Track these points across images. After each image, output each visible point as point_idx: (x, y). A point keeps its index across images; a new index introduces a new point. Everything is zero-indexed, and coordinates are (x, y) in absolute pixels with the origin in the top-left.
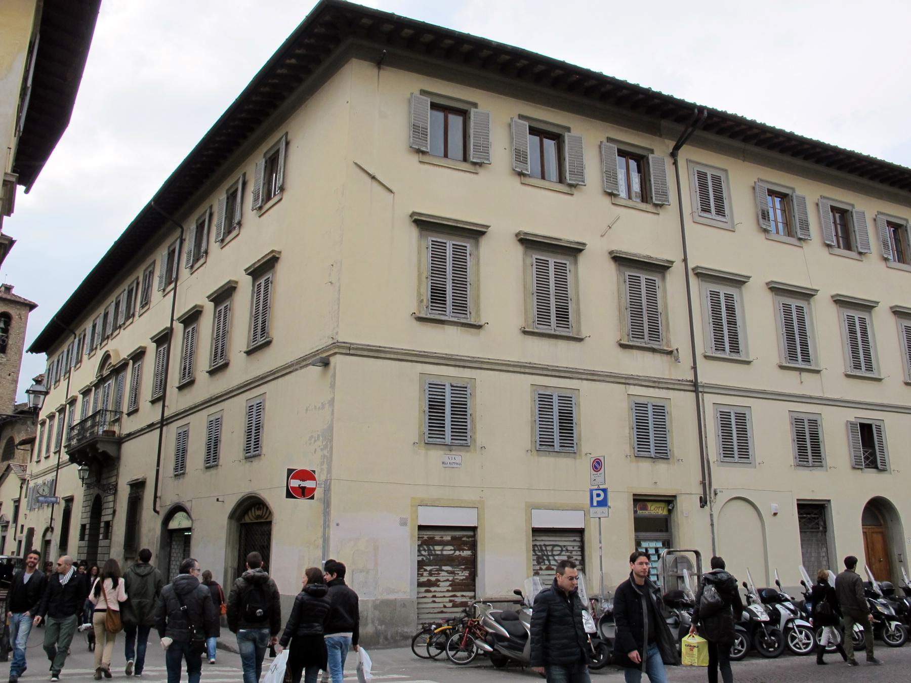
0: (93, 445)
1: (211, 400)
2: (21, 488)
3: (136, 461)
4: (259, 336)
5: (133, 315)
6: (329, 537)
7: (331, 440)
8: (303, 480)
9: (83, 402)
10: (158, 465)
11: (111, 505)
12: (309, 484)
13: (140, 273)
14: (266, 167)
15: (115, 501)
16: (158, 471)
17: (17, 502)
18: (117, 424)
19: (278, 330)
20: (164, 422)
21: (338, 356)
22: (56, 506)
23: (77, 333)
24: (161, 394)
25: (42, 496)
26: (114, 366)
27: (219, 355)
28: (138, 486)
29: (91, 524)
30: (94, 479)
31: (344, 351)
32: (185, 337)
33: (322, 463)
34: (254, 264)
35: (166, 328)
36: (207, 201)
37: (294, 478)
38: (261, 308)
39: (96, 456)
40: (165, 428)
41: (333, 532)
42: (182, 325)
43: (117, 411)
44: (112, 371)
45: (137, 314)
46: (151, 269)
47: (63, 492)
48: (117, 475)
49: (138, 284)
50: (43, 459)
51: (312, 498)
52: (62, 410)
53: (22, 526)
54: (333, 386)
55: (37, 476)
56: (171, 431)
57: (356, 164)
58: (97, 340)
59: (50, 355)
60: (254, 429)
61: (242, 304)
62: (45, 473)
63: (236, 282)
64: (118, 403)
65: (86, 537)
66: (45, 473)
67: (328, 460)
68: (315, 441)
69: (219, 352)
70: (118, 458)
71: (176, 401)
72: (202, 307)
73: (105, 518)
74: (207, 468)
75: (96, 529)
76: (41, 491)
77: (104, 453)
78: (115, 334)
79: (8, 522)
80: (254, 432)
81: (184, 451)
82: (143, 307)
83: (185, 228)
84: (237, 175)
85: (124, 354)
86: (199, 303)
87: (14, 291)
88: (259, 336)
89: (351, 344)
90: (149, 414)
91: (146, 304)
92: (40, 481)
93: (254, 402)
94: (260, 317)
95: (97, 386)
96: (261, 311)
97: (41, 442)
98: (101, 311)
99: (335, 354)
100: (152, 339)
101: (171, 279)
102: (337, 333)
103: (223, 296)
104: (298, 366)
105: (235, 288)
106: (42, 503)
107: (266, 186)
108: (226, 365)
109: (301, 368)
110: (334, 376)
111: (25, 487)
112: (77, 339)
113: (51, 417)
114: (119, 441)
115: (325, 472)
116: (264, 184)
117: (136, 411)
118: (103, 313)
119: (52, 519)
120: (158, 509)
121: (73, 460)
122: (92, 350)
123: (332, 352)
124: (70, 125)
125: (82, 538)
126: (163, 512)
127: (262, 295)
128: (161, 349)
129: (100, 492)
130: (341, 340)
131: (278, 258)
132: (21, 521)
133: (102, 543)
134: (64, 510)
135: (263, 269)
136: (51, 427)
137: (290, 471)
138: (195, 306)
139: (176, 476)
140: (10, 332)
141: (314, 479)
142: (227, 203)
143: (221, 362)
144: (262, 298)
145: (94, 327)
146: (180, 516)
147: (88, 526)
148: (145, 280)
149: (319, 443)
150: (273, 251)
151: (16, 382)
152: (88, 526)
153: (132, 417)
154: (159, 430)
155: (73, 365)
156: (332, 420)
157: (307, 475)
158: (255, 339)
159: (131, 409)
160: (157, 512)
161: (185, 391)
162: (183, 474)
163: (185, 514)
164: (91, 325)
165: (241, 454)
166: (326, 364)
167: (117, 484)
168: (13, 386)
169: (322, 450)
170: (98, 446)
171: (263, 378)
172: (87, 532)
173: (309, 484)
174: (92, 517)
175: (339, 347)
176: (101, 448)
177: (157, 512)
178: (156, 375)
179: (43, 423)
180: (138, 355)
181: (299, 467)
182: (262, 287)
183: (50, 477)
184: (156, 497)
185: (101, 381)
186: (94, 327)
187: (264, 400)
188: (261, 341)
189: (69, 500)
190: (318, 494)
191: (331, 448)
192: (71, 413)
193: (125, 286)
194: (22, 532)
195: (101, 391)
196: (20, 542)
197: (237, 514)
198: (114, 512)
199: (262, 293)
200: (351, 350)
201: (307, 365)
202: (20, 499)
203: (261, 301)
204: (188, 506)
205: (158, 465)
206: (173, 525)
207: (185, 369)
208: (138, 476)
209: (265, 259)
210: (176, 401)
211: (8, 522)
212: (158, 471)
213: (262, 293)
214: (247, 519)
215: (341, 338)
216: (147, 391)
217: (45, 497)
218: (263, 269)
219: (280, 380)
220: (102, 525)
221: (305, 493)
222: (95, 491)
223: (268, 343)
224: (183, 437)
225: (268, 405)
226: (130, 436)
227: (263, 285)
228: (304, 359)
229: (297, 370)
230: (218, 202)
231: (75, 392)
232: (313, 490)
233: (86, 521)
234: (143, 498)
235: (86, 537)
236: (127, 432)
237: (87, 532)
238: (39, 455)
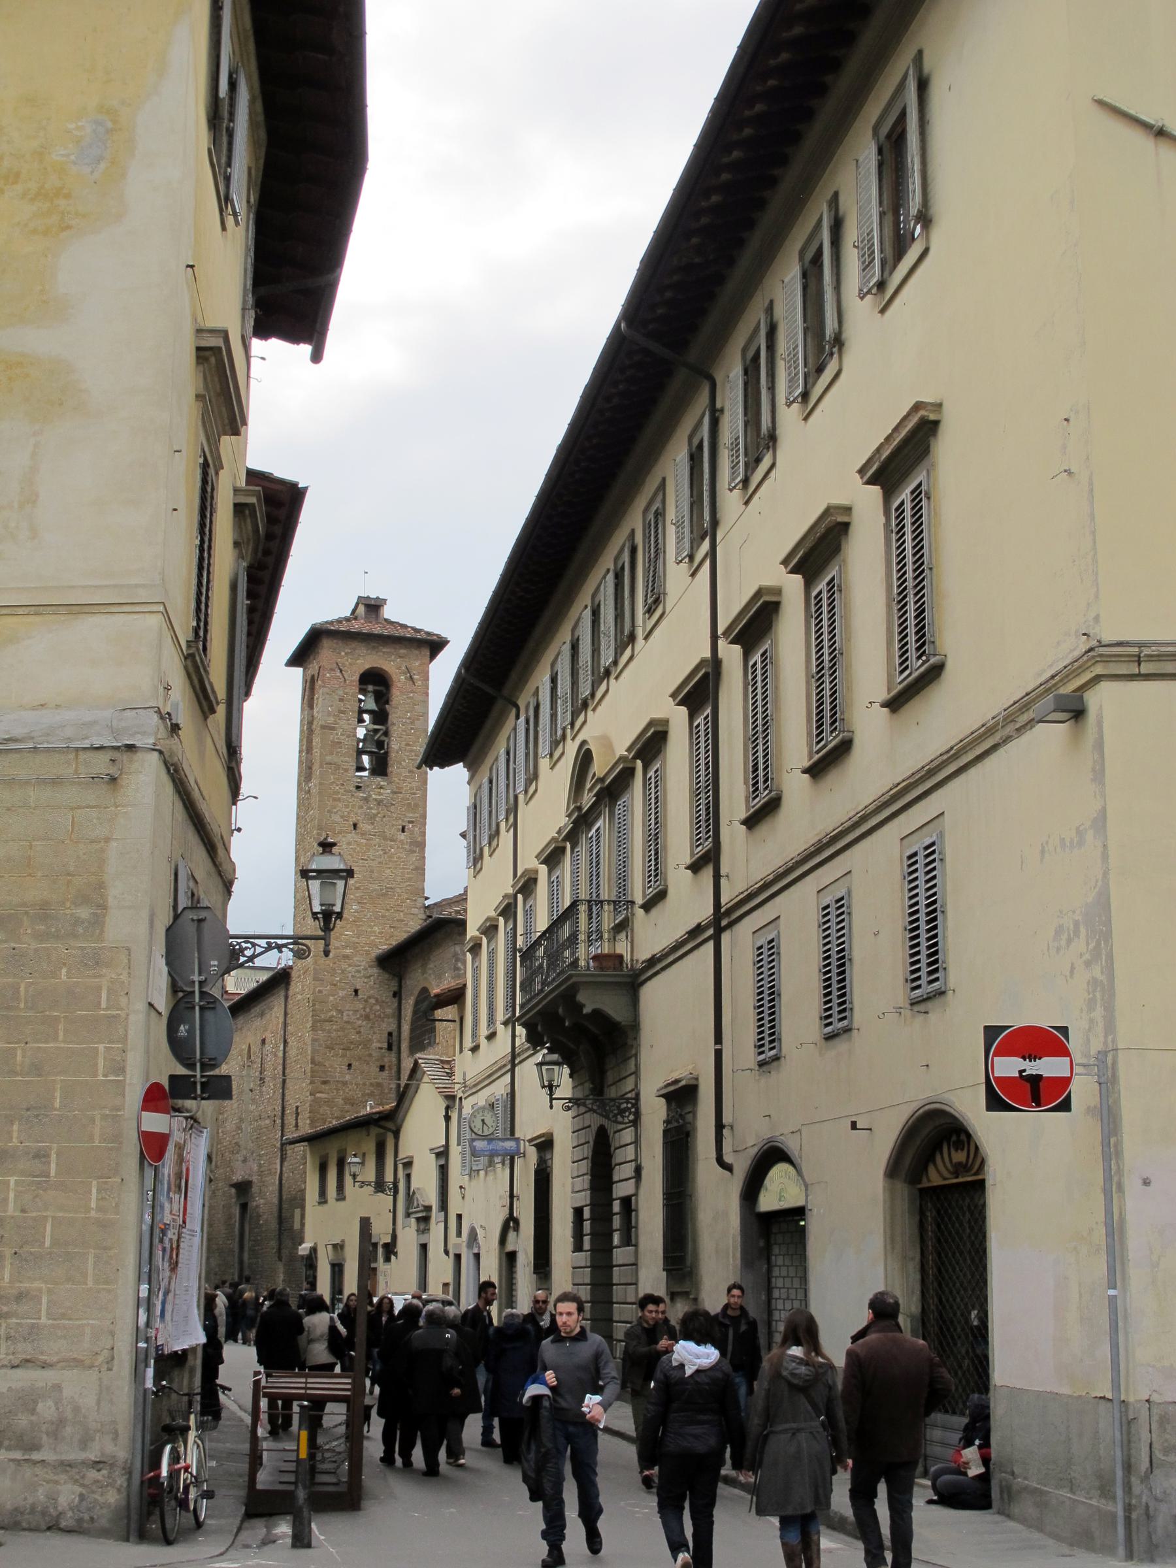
0: (568, 996)
1: (820, 848)
2: (447, 1118)
3: (673, 1033)
4: (912, 654)
5: (632, 638)
6: (1122, 1220)
7: (1107, 936)
8: (1032, 1057)
9: (550, 883)
10: (718, 1039)
11: (630, 1153)
12: (1049, 1067)
13: (635, 521)
14: (881, 165)
15: (636, 1142)
16: (718, 1054)
17: (443, 1154)
18: (623, 935)
19: (956, 634)
20: (722, 920)
21: (1104, 685)
22: (518, 1163)
23: (522, 703)
24: (708, 844)
25: (483, 1137)
26: (602, 780)
27: (827, 720)
28: (681, 1096)
29: (593, 1205)
30: (588, 1085)
31: (1123, 669)
32: (749, 683)
33: (1091, 1004)
34: (878, 450)
35: (703, 662)
36: (759, 293)
37: (1003, 1052)
38: (910, 575)
39: (583, 1028)
40: (726, 937)
41: (1136, 1207)
42: (737, 649)
43: (622, 903)
44: (601, 794)
45: (640, 634)
46: (657, 505)
47: (530, 1124)
48: (636, 1073)
49: (634, 551)
50: (483, 1042)
51: (1065, 1106)
52: (508, 910)
53: (459, 1217)
54: (1099, 775)
55: (476, 1087)
56: (740, 943)
57: (1101, 103)
58: (564, 718)
59: (473, 767)
60: (923, 918)
61: (866, 563)
62: (490, 1078)
63: (848, 510)
64: (622, 879)
65: (587, 1240)
66: (490, 1078)
67: (1104, 993)
68: (1069, 941)
69: (827, 714)
70: (635, 1026)
71: (747, 859)
72: (778, 591)
73: (621, 1190)
74: (829, 1038)
75: (604, 1221)
76: (478, 1125)
77: (597, 1014)
78: (599, 694)
79: (428, 1209)
80: (924, 927)
81: (774, 994)
82: (650, 611)
83: (719, 379)
84: (818, 210)
85: (622, 745)
86: (768, 582)
87: (388, 613)
88: (912, 654)
89: (1141, 645)
90: (689, 902)
91: (657, 601)
92: (481, 1099)
93: (917, 845)
94: (911, 599)
95: (573, 836)
96: (910, 583)
97: (476, 996)
98: (564, 636)
99: (1097, 679)
100: (673, 695)
101: (706, 527)
102: (1097, 619)
103: (819, 552)
104: (1010, 729)
105: (845, 526)
106: (492, 1155)
107: (889, 218)
108: (845, 747)
109: (1020, 731)
110: (1099, 745)
111: (454, 1116)
112: (522, 719)
113: (490, 929)
114: (632, 981)
115: (1100, 1028)
116: (882, 215)
117: (661, 895)
118: (568, 639)
119: (512, 1196)
120: (728, 1158)
121: (535, 1040)
122: (555, 744)
123: (1087, 676)
124: (371, 165)
125: (578, 1247)
126: (742, 1166)
127: (909, 537)
128: (699, 720)
129: (605, 1122)
130: (1108, 638)
131: (936, 424)
132: (454, 1208)
133: (620, 1255)
134: (537, 1172)
135: (904, 459)
136: (492, 954)
137: (991, 1032)
138: (759, 593)
139: (761, 1064)
140: (392, 718)
141: (1064, 1052)
142: (805, 288)
143: (832, 740)
144: (909, 545)
145: (554, 680)
146: (778, 1174)
147: (587, 1213)
148: (647, 537)
149: (1080, 945)
150: (917, 406)
151: (422, 845)
152: (587, 1213)
153: (654, 912)
154: (711, 944)
155: (520, 788)
156: (1106, 874)
157: (1048, 1042)
158: (904, 665)
159: (651, 892)
160: (728, 1168)
161: (763, 829)
162: (777, 1058)
163: (790, 1168)
164: (546, 678)
165: (899, 993)
166: (1077, 713)
167: (637, 1097)
168: (414, 857)
169: (1088, 964)
170: (581, 997)
171: (931, 773)
172: (587, 1225)
173: (1049, 1067)
174: (594, 1188)
175: (1106, 659)
176: (589, 1002)
177: (728, 1168)
178: (696, 793)
179: (476, 948)
180: (652, 743)
181: (1018, 1019)
182: (908, 513)
183: (500, 1088)
184: (720, 1126)
185: (582, 822)
186: (554, 680)
187: (941, 835)
188: (917, 667)
189: (545, 1145)
190: (1082, 1091)
191: (1110, 957)
192: (529, 913)
193: (607, 562)
194: (459, 1234)
195: (583, 848)
196: (458, 1257)
197: (907, 1161)
198: (638, 1170)
199: (908, 529)
200: (1143, 663)
201: (1031, 723)
202: (447, 1146)
203: (909, 552)
204: (791, 1145)
205: (718, 1039)
206: (768, 1202)
207: (755, 769)
208: (680, 1072)
209: (903, 433)
210: (747, 859)
211: (428, 1209)
212: (718, 1054)
213: (908, 529)
214: (935, 1177)
215: (1109, 635)
216: (680, 846)
217: (489, 1139)
218: (904, 459)
219: (973, 771)
220: (616, 1207)
221: (1042, 1094)
222: (595, 1120)
223: (935, 672)
224: (768, 956)
225: (951, 850)
226: (656, 964)
227: (908, 506)
228: (1024, 704)
229: (1007, 740)
230: (784, 288)
231: (529, 861)
232: (1066, 1081)
233: (584, 1199)
234: (695, 1129)
235: (587, 1240)
236: (647, 955)
237: (587, 1225)
238: (475, 1035)
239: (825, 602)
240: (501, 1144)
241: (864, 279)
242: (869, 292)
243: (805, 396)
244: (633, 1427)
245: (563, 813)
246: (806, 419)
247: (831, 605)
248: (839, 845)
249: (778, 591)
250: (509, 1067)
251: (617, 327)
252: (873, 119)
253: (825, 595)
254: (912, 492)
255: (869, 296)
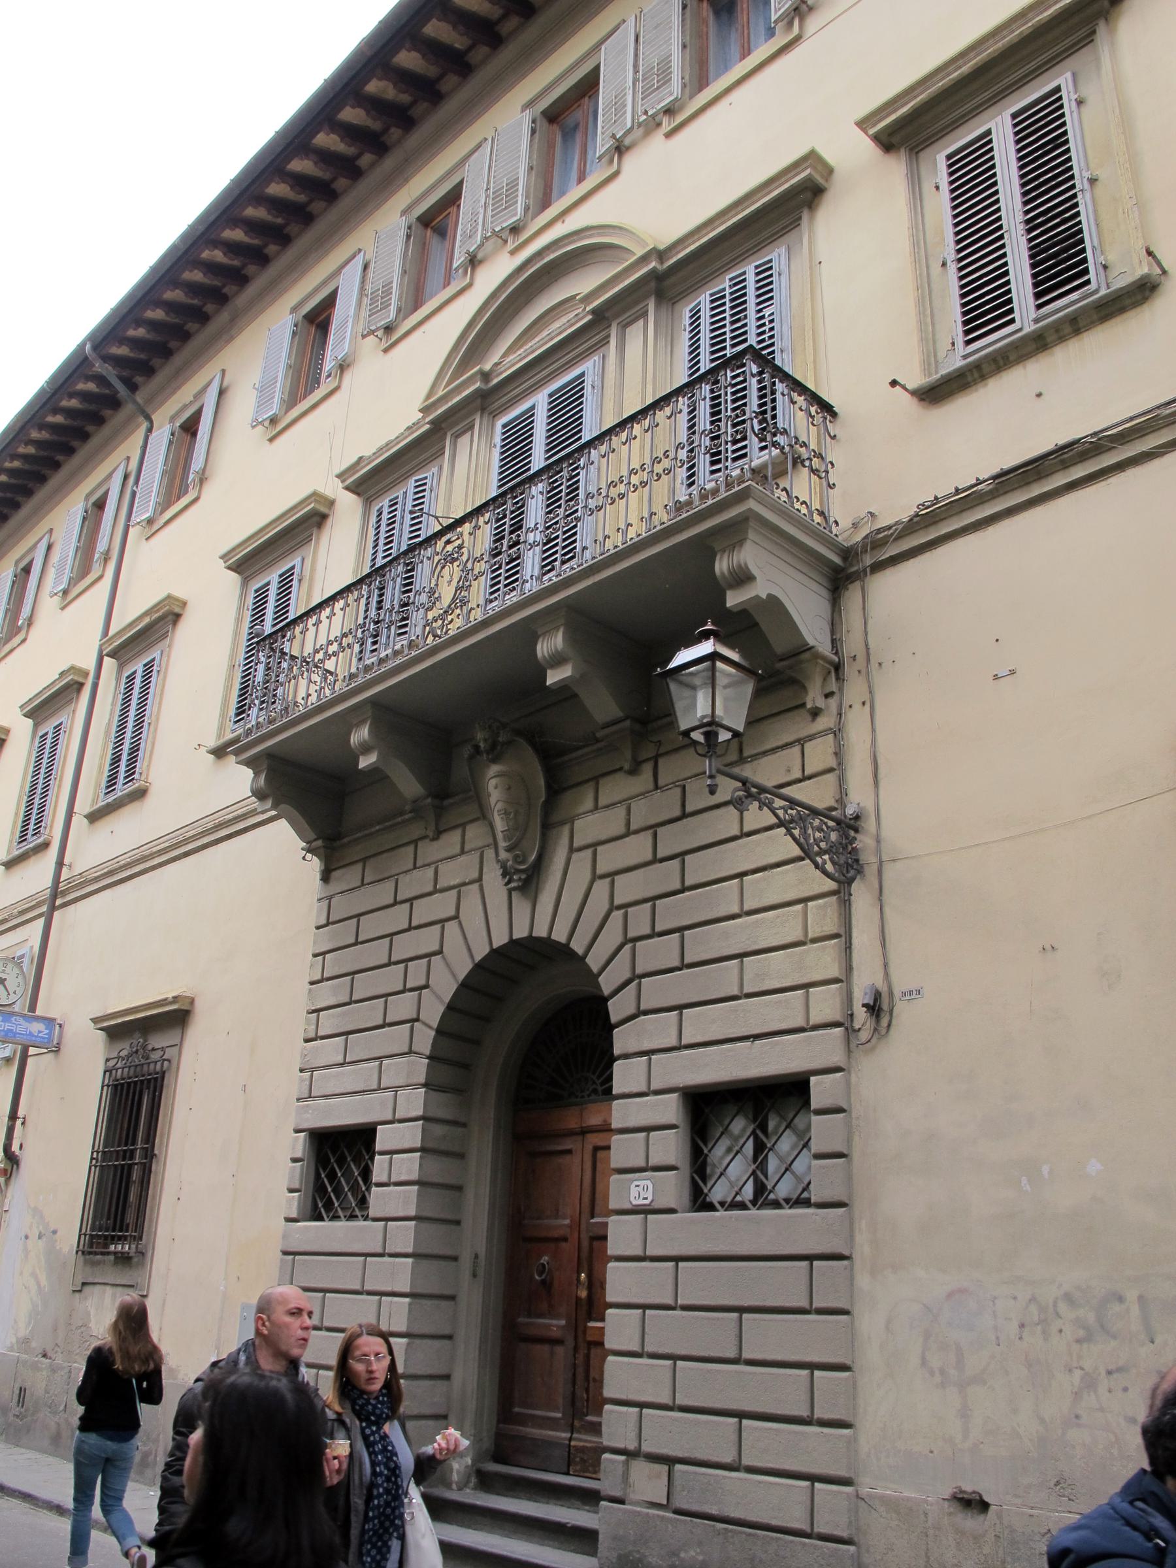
72: (331, 503)
154: (41, 921)
239: (49, 741)
240: (25, 1024)
241: (56, 584)
242: (261, 423)
243: (65, 592)
244: (71, 1492)
245: (418, 401)
246: (63, 608)
247: (55, 744)
248: (241, 825)
249: (331, 503)
250: (44, 908)
251: (82, 346)
252: (172, 412)
253: (50, 736)
254: (145, 665)
255: (260, 427)
